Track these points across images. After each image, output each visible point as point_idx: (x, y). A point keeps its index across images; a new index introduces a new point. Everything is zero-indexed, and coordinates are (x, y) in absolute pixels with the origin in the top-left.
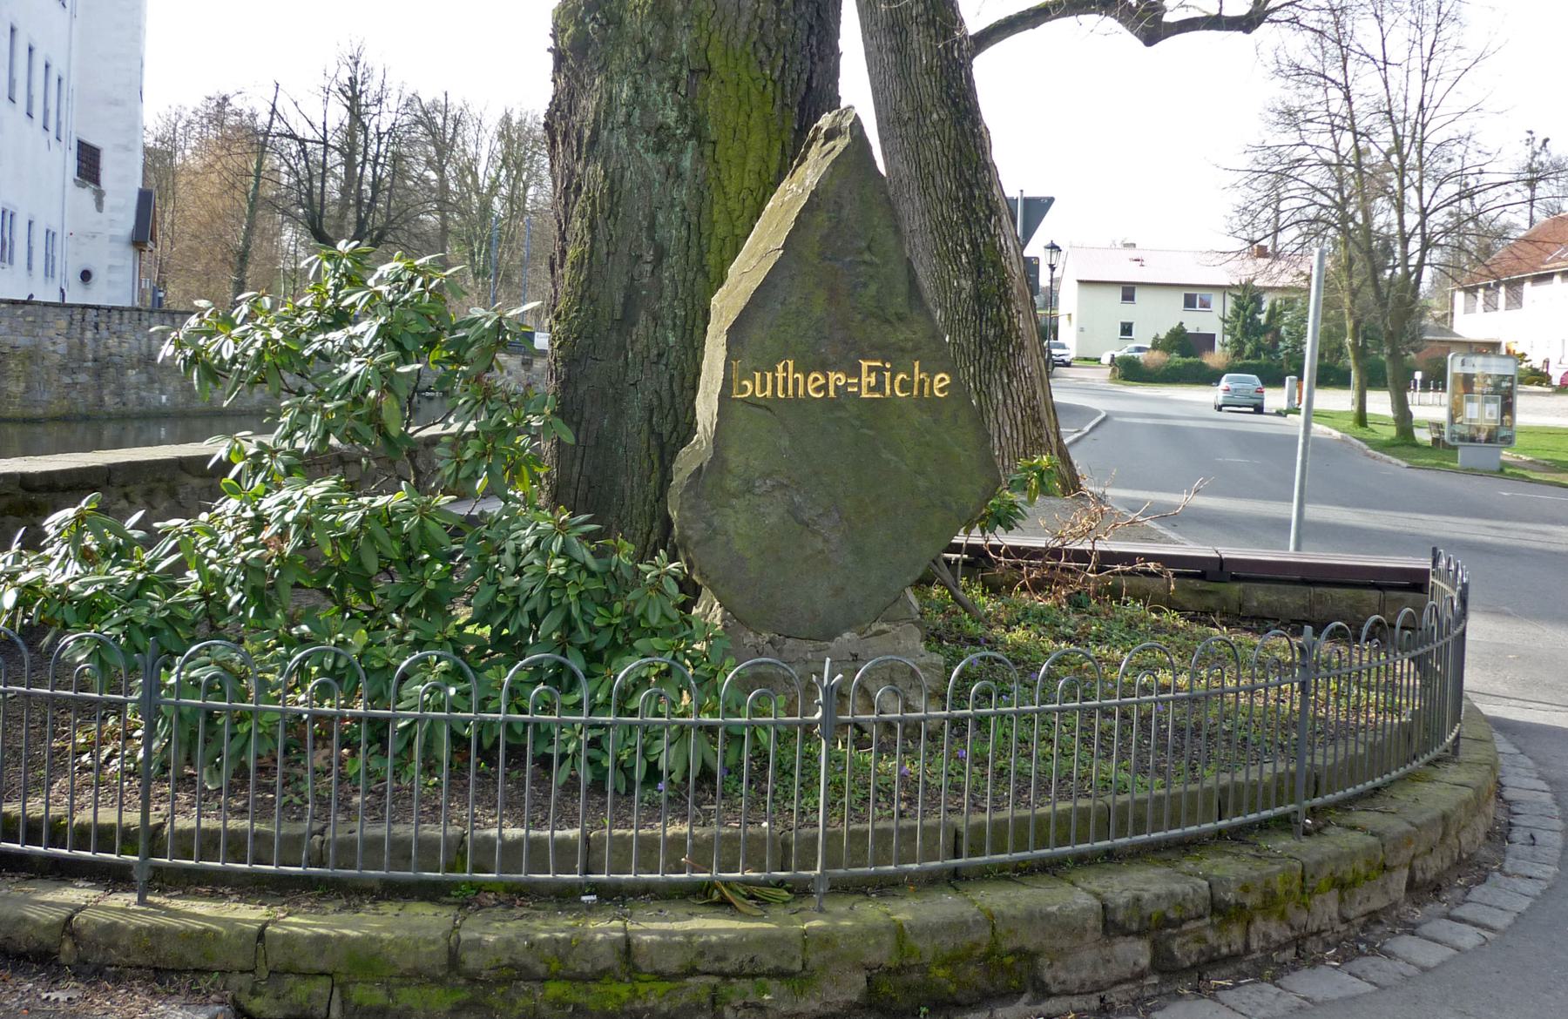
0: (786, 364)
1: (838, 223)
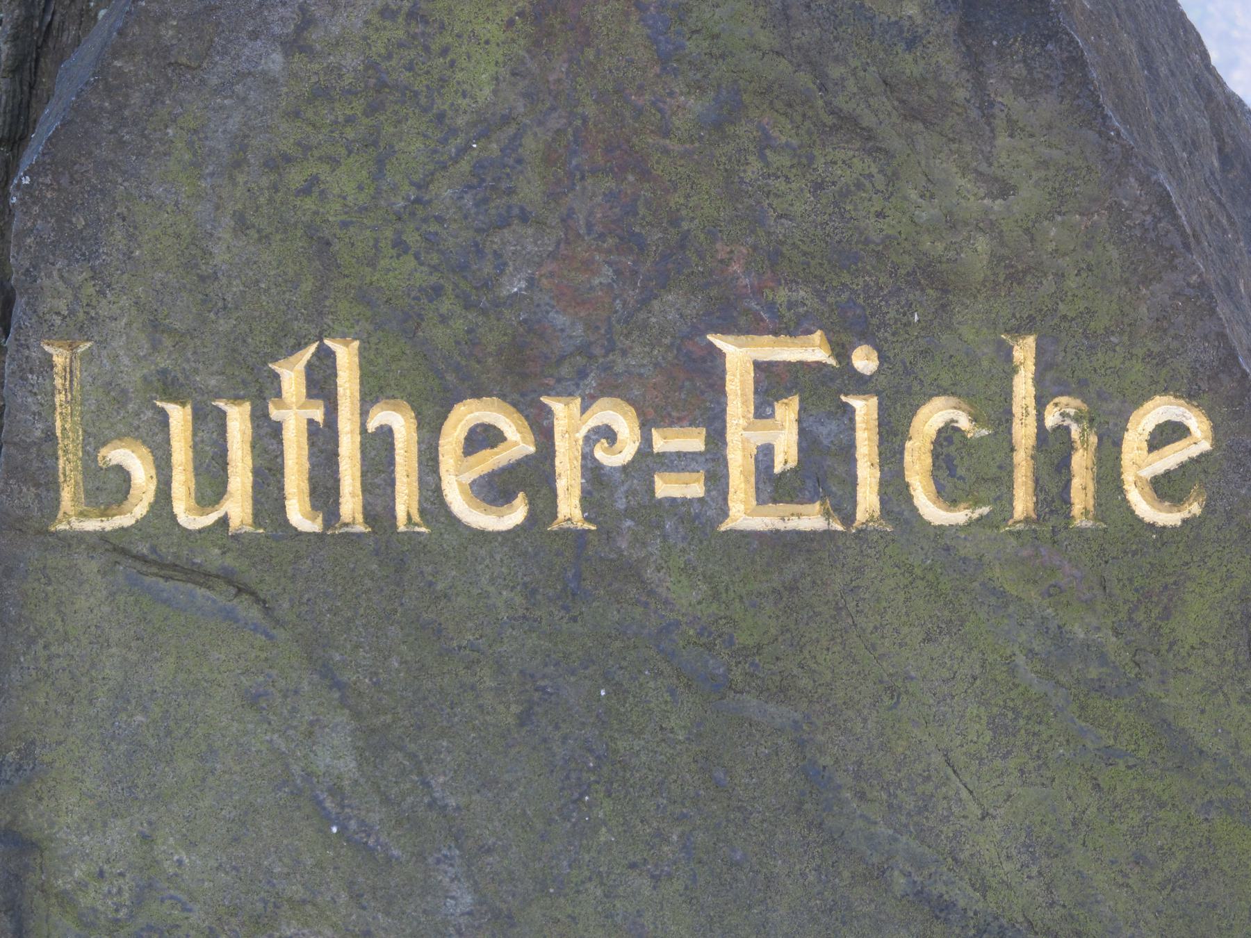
0: (325, 360)
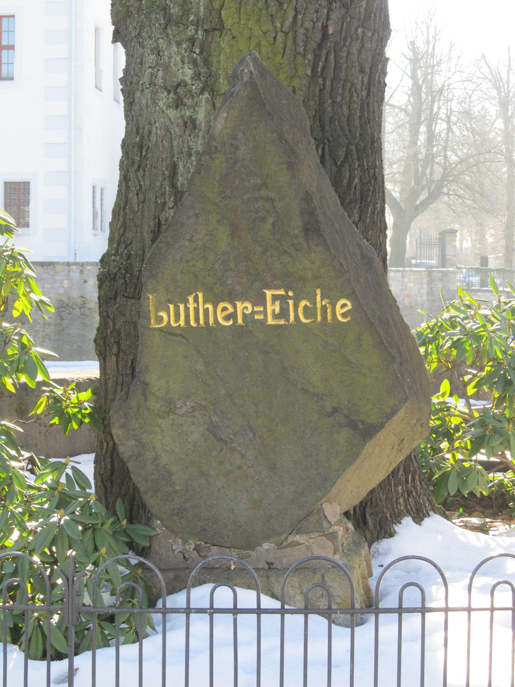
0: (197, 296)
1: (235, 163)
